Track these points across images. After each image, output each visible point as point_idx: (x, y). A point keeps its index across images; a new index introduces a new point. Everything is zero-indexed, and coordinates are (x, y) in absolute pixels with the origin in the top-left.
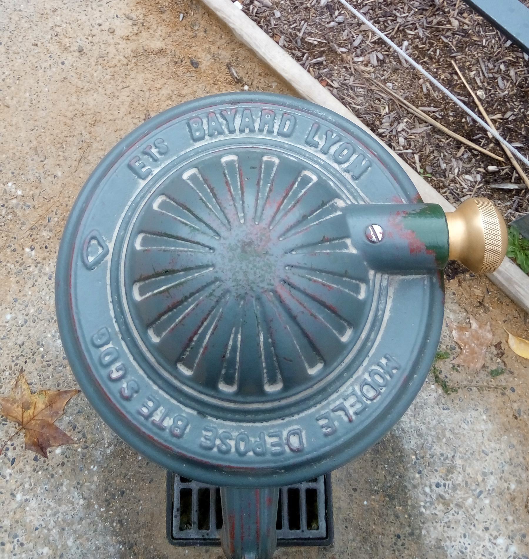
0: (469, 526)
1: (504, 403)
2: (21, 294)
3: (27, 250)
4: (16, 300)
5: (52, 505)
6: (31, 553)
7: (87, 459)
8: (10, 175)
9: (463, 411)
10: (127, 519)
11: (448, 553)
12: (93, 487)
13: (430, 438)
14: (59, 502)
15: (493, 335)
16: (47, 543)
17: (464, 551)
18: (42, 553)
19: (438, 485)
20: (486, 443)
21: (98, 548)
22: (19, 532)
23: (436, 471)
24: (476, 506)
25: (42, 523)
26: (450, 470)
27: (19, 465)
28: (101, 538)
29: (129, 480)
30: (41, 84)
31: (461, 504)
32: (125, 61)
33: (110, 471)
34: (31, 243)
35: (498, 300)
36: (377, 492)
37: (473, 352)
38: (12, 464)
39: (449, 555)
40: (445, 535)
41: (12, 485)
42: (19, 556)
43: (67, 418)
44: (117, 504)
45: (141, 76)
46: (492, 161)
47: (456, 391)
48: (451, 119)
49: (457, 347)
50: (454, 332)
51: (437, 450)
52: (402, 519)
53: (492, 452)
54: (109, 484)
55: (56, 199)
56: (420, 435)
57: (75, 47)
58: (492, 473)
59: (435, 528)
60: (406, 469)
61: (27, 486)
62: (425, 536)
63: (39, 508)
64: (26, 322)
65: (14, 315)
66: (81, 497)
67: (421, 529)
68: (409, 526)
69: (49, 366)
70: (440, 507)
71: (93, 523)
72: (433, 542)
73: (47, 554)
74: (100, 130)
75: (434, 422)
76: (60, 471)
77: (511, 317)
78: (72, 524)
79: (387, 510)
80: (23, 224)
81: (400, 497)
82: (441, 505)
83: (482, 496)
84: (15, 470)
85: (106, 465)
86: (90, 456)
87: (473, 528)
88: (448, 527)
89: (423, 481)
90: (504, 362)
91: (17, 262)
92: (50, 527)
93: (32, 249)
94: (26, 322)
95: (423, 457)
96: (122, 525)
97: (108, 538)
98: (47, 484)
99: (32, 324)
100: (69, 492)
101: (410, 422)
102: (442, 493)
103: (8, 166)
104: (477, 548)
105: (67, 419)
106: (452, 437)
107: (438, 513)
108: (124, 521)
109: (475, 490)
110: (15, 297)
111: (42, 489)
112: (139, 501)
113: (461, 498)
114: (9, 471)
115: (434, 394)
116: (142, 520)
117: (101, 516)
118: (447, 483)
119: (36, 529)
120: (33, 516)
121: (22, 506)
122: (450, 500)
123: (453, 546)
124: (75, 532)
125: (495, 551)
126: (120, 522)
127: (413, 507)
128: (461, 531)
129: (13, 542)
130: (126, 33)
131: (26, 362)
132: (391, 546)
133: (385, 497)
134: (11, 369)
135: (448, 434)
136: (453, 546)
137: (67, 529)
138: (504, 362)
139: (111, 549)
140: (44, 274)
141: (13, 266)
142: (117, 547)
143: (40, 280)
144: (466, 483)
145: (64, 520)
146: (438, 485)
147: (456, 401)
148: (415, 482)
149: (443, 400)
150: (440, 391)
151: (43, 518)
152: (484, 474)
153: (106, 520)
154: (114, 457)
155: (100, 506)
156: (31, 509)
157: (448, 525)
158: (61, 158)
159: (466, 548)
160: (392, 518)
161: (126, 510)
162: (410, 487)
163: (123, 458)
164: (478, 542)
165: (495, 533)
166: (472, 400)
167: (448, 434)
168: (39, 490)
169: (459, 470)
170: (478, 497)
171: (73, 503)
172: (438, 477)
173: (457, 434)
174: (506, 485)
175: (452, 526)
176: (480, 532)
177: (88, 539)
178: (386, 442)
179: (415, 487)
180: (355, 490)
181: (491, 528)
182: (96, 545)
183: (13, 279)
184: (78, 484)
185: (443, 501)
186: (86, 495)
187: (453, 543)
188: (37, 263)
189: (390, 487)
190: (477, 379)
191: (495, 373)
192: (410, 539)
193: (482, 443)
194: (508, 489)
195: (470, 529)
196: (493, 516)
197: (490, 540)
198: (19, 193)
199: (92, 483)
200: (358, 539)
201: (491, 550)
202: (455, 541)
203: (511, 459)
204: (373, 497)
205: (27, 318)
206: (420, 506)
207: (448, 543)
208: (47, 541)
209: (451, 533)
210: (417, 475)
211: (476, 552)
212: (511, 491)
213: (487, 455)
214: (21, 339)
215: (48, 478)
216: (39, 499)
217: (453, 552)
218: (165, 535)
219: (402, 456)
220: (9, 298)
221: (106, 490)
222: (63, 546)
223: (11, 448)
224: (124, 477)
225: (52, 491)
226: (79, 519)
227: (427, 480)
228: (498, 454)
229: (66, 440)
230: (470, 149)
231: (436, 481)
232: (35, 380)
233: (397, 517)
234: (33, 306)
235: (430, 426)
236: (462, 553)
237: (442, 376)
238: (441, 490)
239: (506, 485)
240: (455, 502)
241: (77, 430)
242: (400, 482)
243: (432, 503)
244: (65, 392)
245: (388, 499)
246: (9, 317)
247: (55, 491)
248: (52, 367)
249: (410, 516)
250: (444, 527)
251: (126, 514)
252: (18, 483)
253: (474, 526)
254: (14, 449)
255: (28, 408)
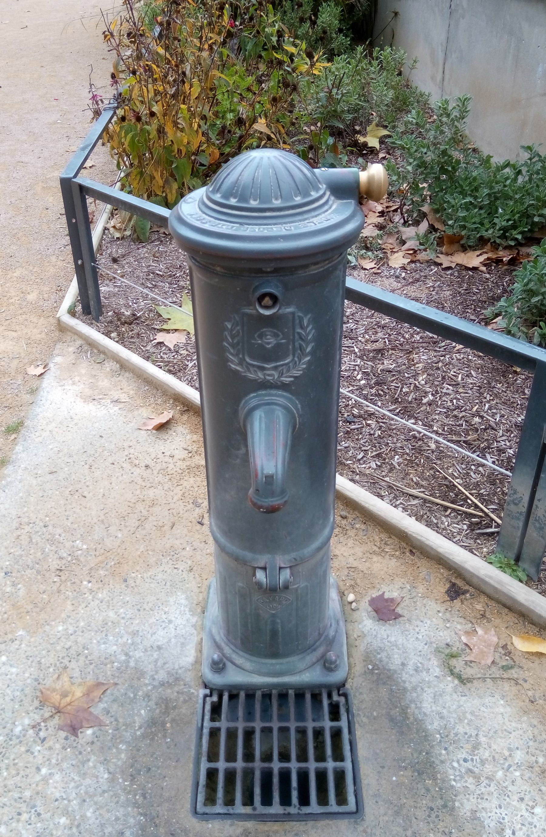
0: (503, 797)
1: (519, 691)
2: (74, 613)
3: (85, 583)
4: (69, 617)
5: (76, 778)
6: (47, 823)
7: (116, 739)
8: (79, 536)
9: (480, 697)
10: (151, 794)
11: (485, 823)
12: (120, 763)
13: (452, 720)
14: (84, 775)
15: (499, 639)
16: (66, 813)
17: (501, 821)
18: (59, 823)
19: (465, 760)
20: (508, 723)
21: (117, 819)
22: (38, 803)
23: (462, 747)
24: (507, 778)
25: (63, 794)
26: (476, 747)
27: (49, 743)
28: (122, 810)
29: (156, 758)
30: (113, 484)
31: (491, 777)
32: (180, 472)
33: (138, 750)
34: (88, 578)
35: (497, 612)
36: (406, 768)
37: (482, 652)
38: (42, 743)
39: (487, 826)
40: (480, 807)
41: (40, 760)
42: (34, 826)
43: (102, 705)
44: (141, 779)
45: (192, 480)
46: (475, 516)
47: (472, 682)
48: (438, 495)
49: (467, 648)
50: (463, 638)
51: (460, 729)
52: (433, 792)
53: (514, 731)
54: (136, 761)
55: (114, 550)
56: (442, 718)
57: (143, 465)
58: (517, 748)
59: (468, 800)
60: (432, 747)
61: (54, 761)
62: (459, 808)
63: (63, 781)
64: (75, 632)
65: (65, 627)
66: (106, 771)
67: (453, 801)
68: (441, 798)
69: (91, 664)
70: (471, 780)
71: (116, 795)
72: (469, 814)
73: (64, 824)
74: (156, 509)
75: (454, 707)
76: (89, 749)
77: (512, 624)
78: (95, 795)
79: (417, 784)
80: (84, 566)
81: (429, 771)
82: (471, 778)
83: (511, 769)
84: (44, 747)
85: (134, 745)
86: (120, 737)
87: (508, 799)
88: (482, 799)
89: (450, 757)
90: (512, 659)
91: (75, 591)
92: (71, 798)
93: (89, 582)
94: (75, 632)
95: (447, 736)
96: (145, 798)
97: (130, 809)
98: (74, 760)
99: (81, 634)
100: (95, 767)
101: (431, 707)
102: (471, 767)
103: (78, 531)
104: (515, 818)
105: (102, 705)
106: (473, 718)
107: (469, 786)
108: (147, 795)
109: (504, 764)
110: (68, 614)
111: (68, 764)
112: (165, 777)
113: (491, 771)
114: (39, 748)
115: (451, 685)
116: (166, 794)
117: (125, 789)
118: (475, 758)
119: (57, 800)
120: (55, 788)
121: (45, 780)
122: (480, 774)
123: (489, 817)
124: (96, 803)
125: (535, 821)
126: (144, 796)
127: (443, 781)
128: (495, 802)
129: (30, 812)
130: (182, 457)
131: (70, 661)
132: (425, 819)
133: (413, 772)
134: (55, 666)
135: (469, 716)
136: (489, 817)
137: (88, 800)
138: (512, 659)
139: (132, 821)
140: (97, 599)
141: (70, 594)
142: (138, 818)
143: (92, 603)
144: (494, 757)
145: (86, 793)
146: (465, 760)
147: (472, 690)
148: (443, 758)
149: (460, 689)
150: (456, 682)
151: (64, 790)
152: (510, 749)
153: (129, 793)
154: (144, 738)
155: (125, 780)
156: (54, 782)
157: (481, 797)
158: (123, 526)
159: (503, 819)
160: (423, 791)
161: (150, 785)
162: (437, 762)
163: (152, 739)
164: (515, 812)
165: (531, 803)
166: (488, 688)
167: (469, 716)
168: (65, 765)
169: (484, 746)
170: (508, 770)
171: (97, 777)
172: (465, 753)
173: (477, 716)
174: (534, 759)
175: (485, 798)
176: (515, 803)
177: (108, 811)
178: (410, 724)
179: (442, 762)
180: (383, 767)
181: (527, 798)
182: (116, 815)
183: (69, 602)
184: (105, 760)
185: (473, 775)
186: (111, 770)
187: (489, 814)
188: (91, 591)
189: (418, 763)
190: (490, 672)
191: (505, 668)
192: (444, 811)
193: (504, 723)
194: (537, 762)
195: (504, 800)
196: (526, 787)
197: (527, 810)
198: (85, 547)
199: (119, 760)
200: (390, 812)
201: (530, 819)
202: (490, 812)
203: (534, 737)
204: (402, 773)
205: (77, 629)
206: (450, 780)
207: (484, 814)
208: (65, 812)
209: (485, 804)
210: (444, 752)
211: (514, 822)
212: (540, 764)
213: (511, 733)
214: (69, 644)
215: (76, 755)
216: (64, 773)
217: (490, 823)
218: (189, 810)
219: (426, 736)
220: (63, 615)
221: (132, 766)
222: (81, 816)
223: (44, 729)
224: (152, 756)
225: (78, 766)
226: (101, 792)
227: (454, 756)
228: (521, 732)
229: (98, 723)
230: (454, 510)
231: (463, 756)
232: (76, 674)
233: (428, 790)
234: (84, 620)
235: (451, 710)
236: (501, 823)
237: (456, 671)
238: (469, 765)
239: (534, 759)
240: (485, 776)
241: (110, 715)
242: (427, 758)
243: (462, 777)
244: (103, 684)
245: (416, 774)
246: (60, 628)
247: (81, 766)
248: (94, 665)
249: (441, 789)
250: (477, 798)
251: (150, 789)
252: (45, 759)
253: (508, 796)
254: (47, 730)
255: (66, 696)
